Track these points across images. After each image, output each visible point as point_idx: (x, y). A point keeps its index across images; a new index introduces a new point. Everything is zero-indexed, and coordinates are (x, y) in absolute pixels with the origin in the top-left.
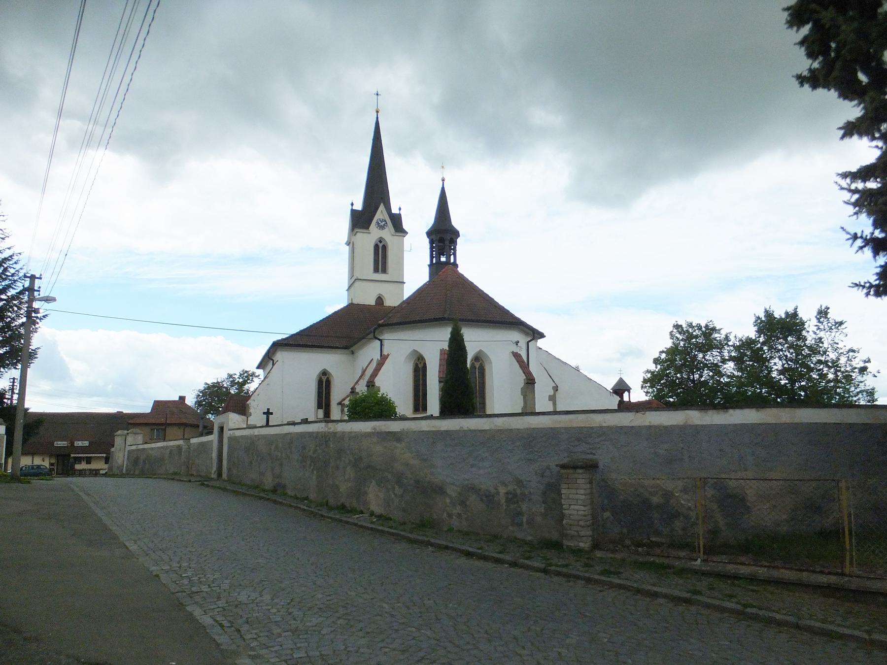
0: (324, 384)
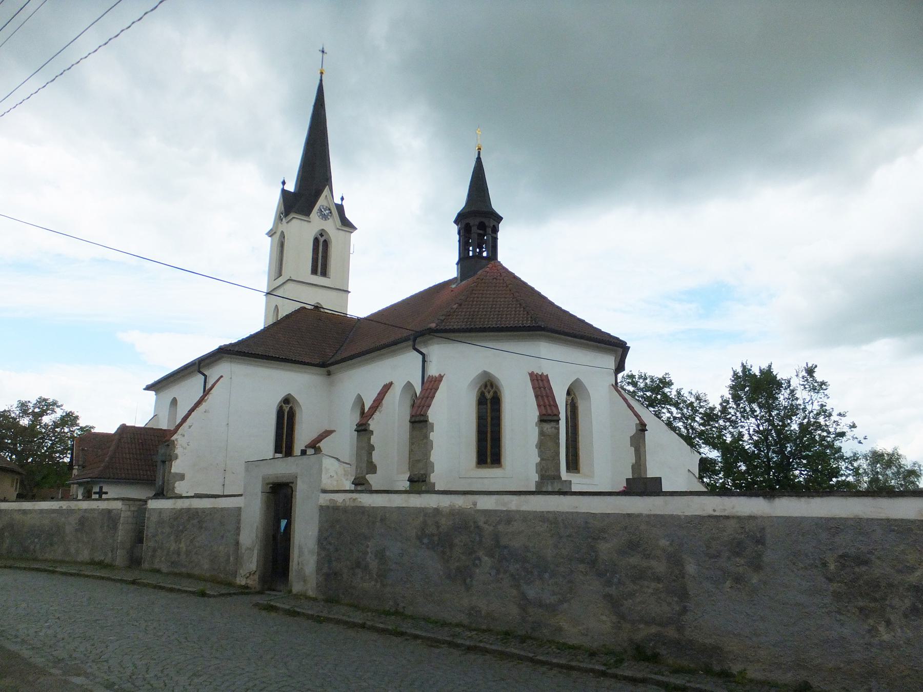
0: (286, 417)
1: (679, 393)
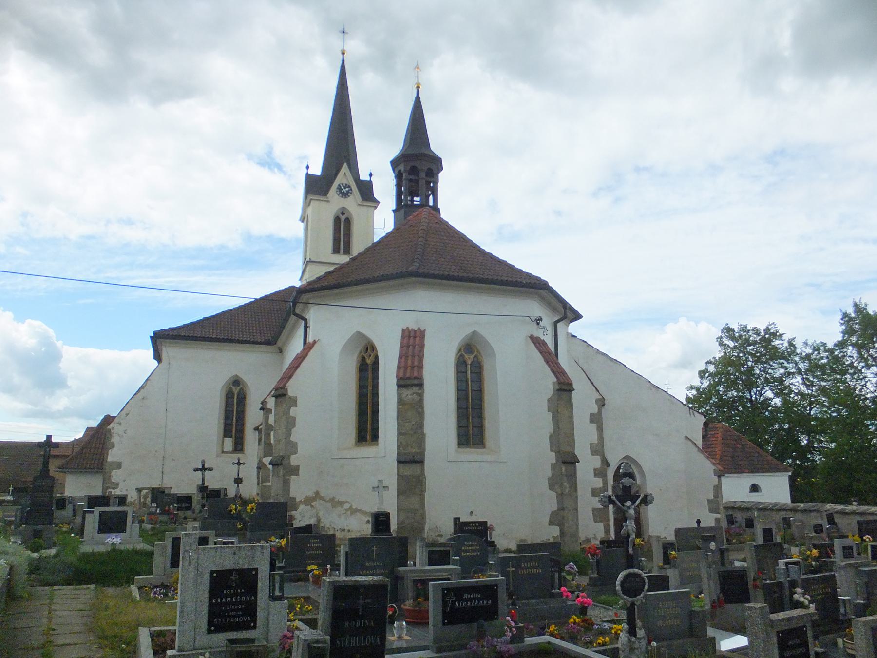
0: (235, 400)
1: (791, 343)
